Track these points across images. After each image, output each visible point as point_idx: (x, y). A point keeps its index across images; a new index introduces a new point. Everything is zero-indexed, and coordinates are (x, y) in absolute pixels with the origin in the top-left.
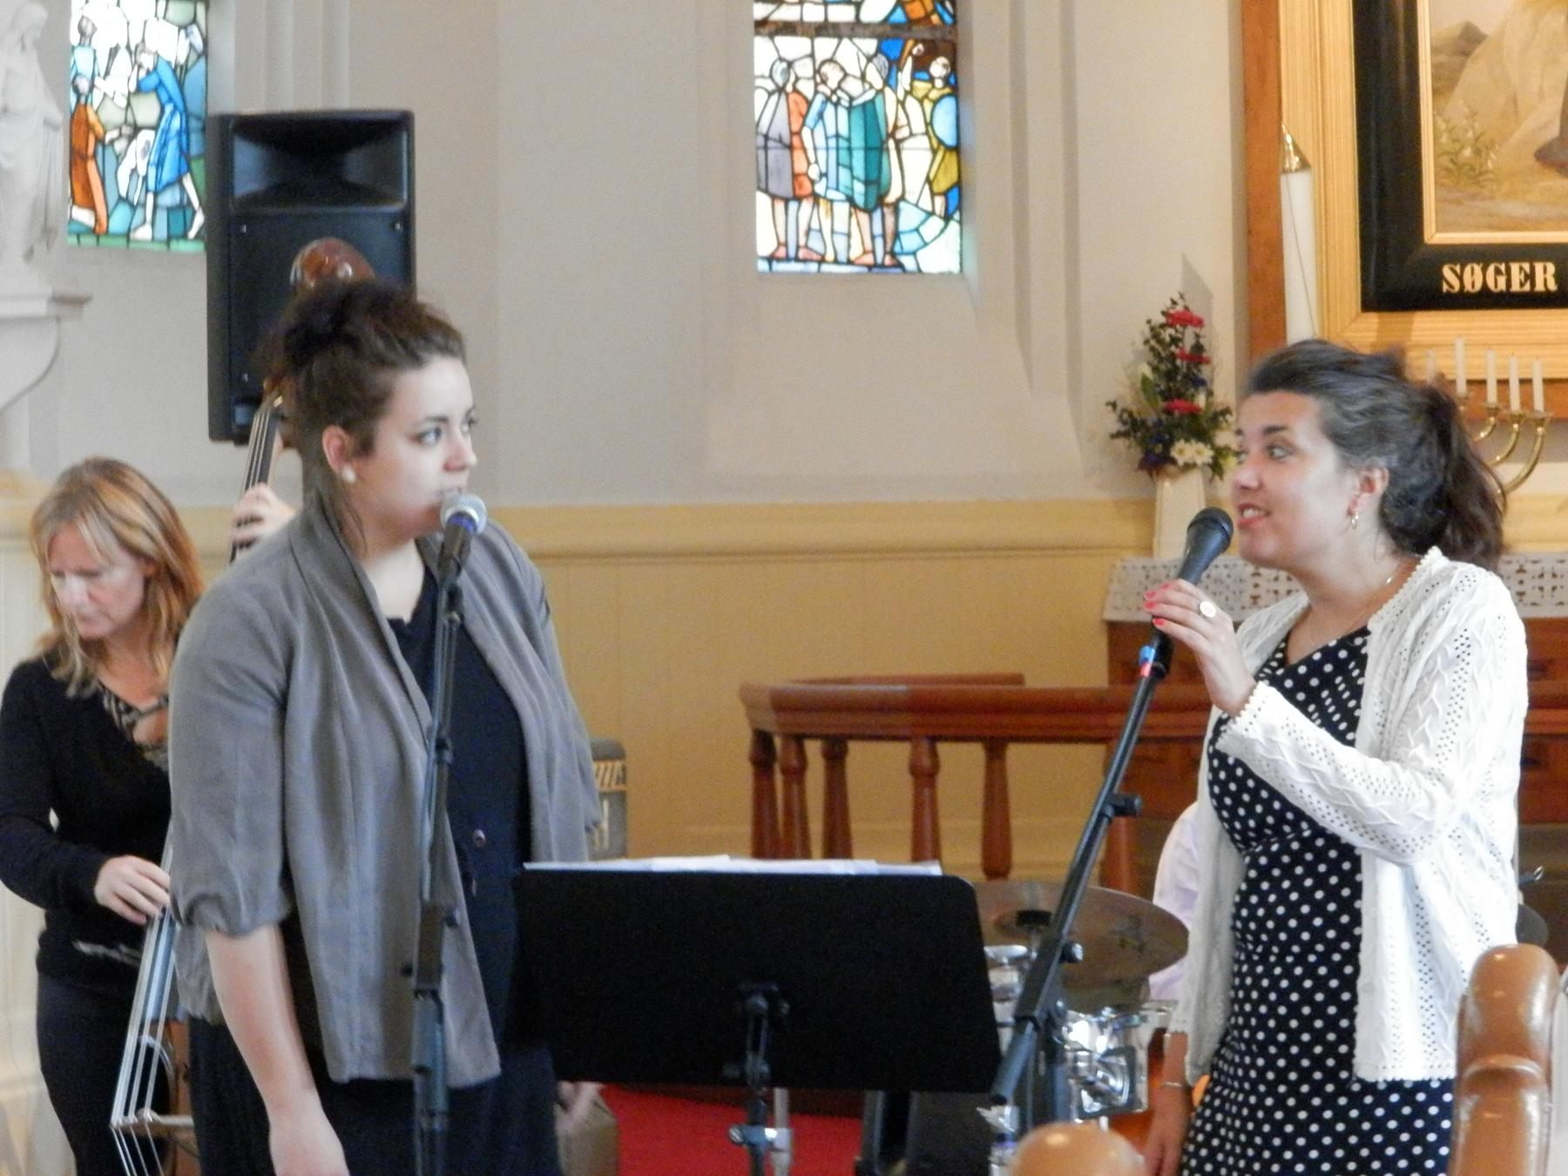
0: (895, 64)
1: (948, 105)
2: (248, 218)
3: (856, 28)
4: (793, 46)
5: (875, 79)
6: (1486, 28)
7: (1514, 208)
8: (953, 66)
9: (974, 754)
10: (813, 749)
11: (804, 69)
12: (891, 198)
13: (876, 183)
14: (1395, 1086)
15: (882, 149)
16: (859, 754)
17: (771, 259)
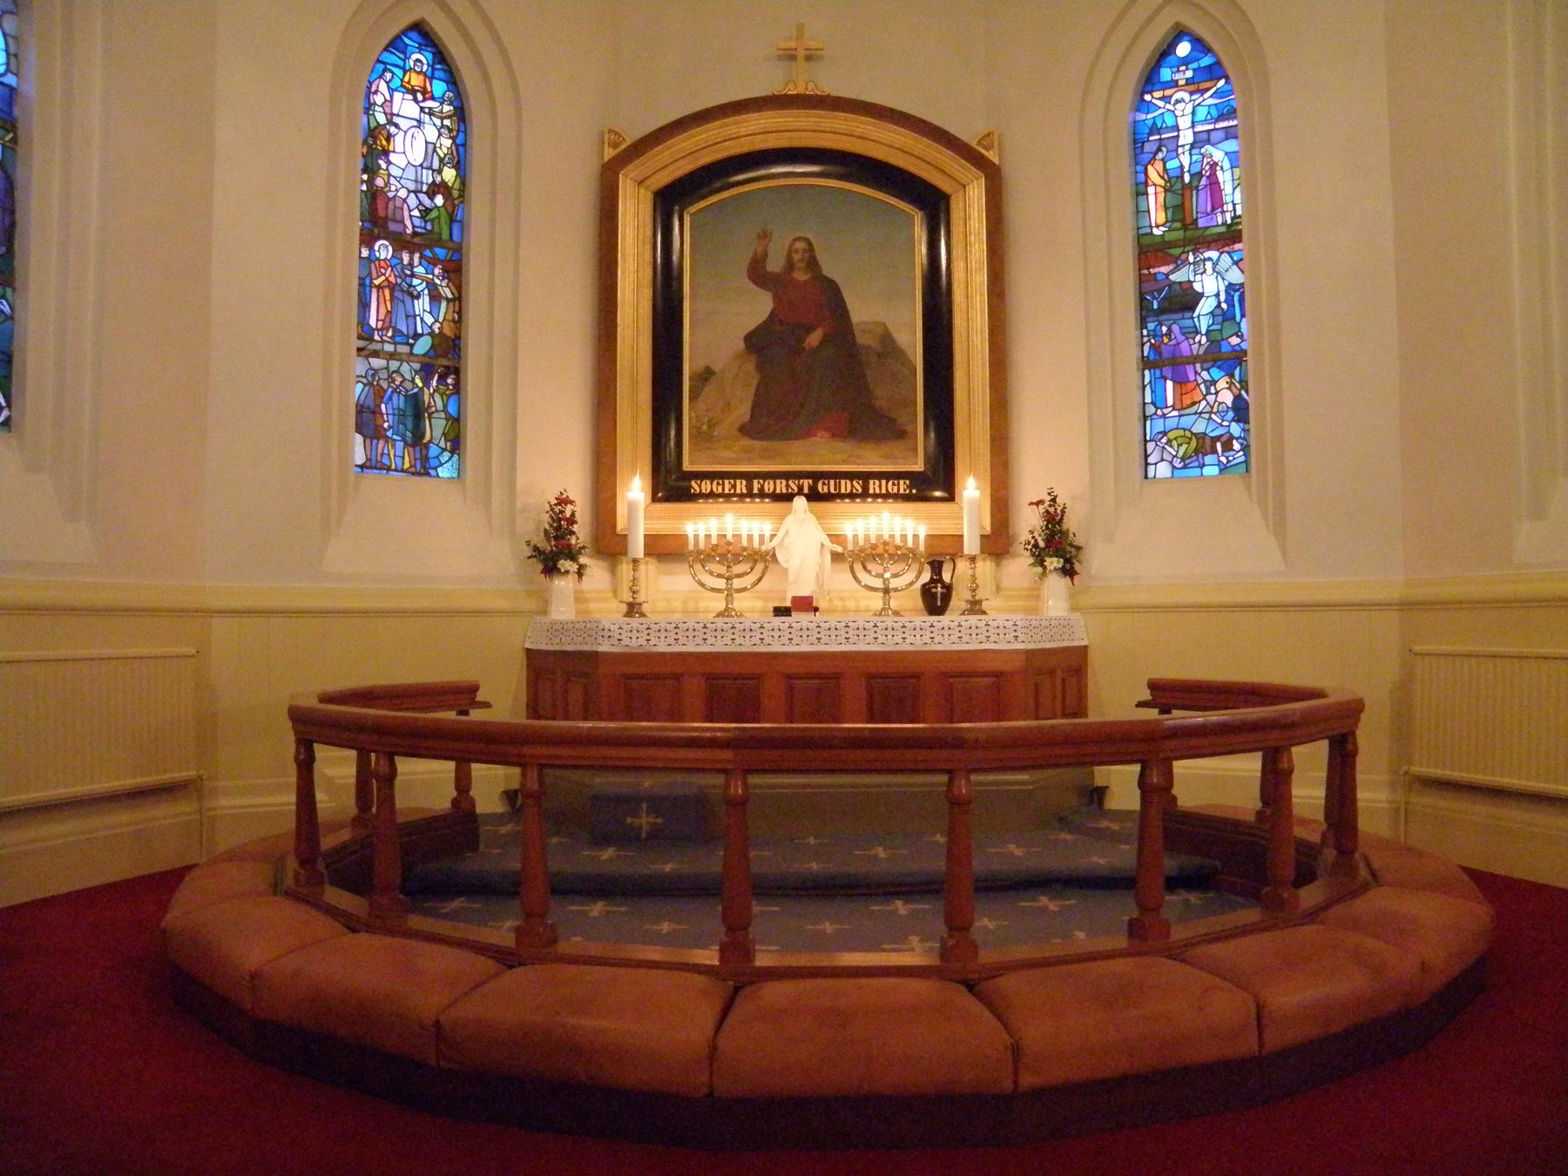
6: (717, 368)
11: (384, 375)
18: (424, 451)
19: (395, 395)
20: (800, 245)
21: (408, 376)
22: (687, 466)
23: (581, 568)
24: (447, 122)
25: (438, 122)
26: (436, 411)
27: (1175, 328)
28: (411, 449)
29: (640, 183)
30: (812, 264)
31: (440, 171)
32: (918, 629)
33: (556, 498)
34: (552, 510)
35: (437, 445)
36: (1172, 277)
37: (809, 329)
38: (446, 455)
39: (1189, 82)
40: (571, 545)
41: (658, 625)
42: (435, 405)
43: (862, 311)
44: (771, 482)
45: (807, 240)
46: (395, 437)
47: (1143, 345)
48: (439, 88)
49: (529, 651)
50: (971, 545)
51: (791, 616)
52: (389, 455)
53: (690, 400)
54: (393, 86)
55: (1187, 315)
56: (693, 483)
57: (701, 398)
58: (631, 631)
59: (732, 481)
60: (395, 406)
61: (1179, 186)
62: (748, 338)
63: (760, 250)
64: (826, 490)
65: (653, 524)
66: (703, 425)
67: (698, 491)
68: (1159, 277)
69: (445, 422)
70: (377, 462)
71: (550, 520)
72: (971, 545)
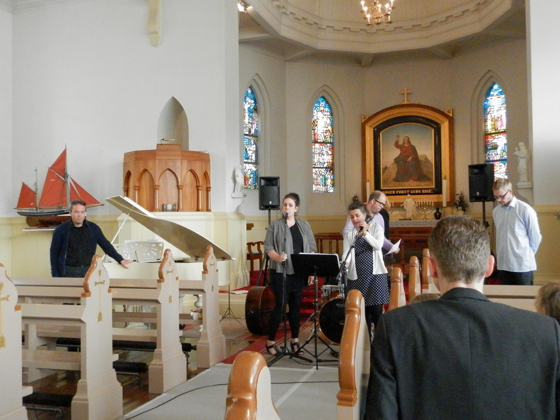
0: (327, 171)
1: (332, 175)
2: (263, 188)
3: (323, 168)
4: (317, 169)
5: (325, 173)
6: (388, 166)
7: (391, 185)
8: (333, 171)
9: (335, 241)
10: (319, 240)
11: (318, 172)
12: (327, 184)
13: (325, 183)
14: (379, 275)
15: (326, 180)
16: (323, 241)
17: (315, 191)
20: (406, 138)
21: (323, 172)
24: (329, 117)
25: (327, 117)
27: (493, 153)
29: (370, 127)
30: (409, 142)
31: (327, 127)
36: (493, 141)
37: (409, 157)
39: (497, 95)
43: (421, 152)
45: (408, 137)
47: (486, 157)
48: (327, 109)
50: (444, 205)
51: (85, 221)
54: (317, 111)
55: (496, 150)
61: (494, 120)
62: (395, 159)
63: (397, 140)
68: (490, 141)
72: (444, 205)
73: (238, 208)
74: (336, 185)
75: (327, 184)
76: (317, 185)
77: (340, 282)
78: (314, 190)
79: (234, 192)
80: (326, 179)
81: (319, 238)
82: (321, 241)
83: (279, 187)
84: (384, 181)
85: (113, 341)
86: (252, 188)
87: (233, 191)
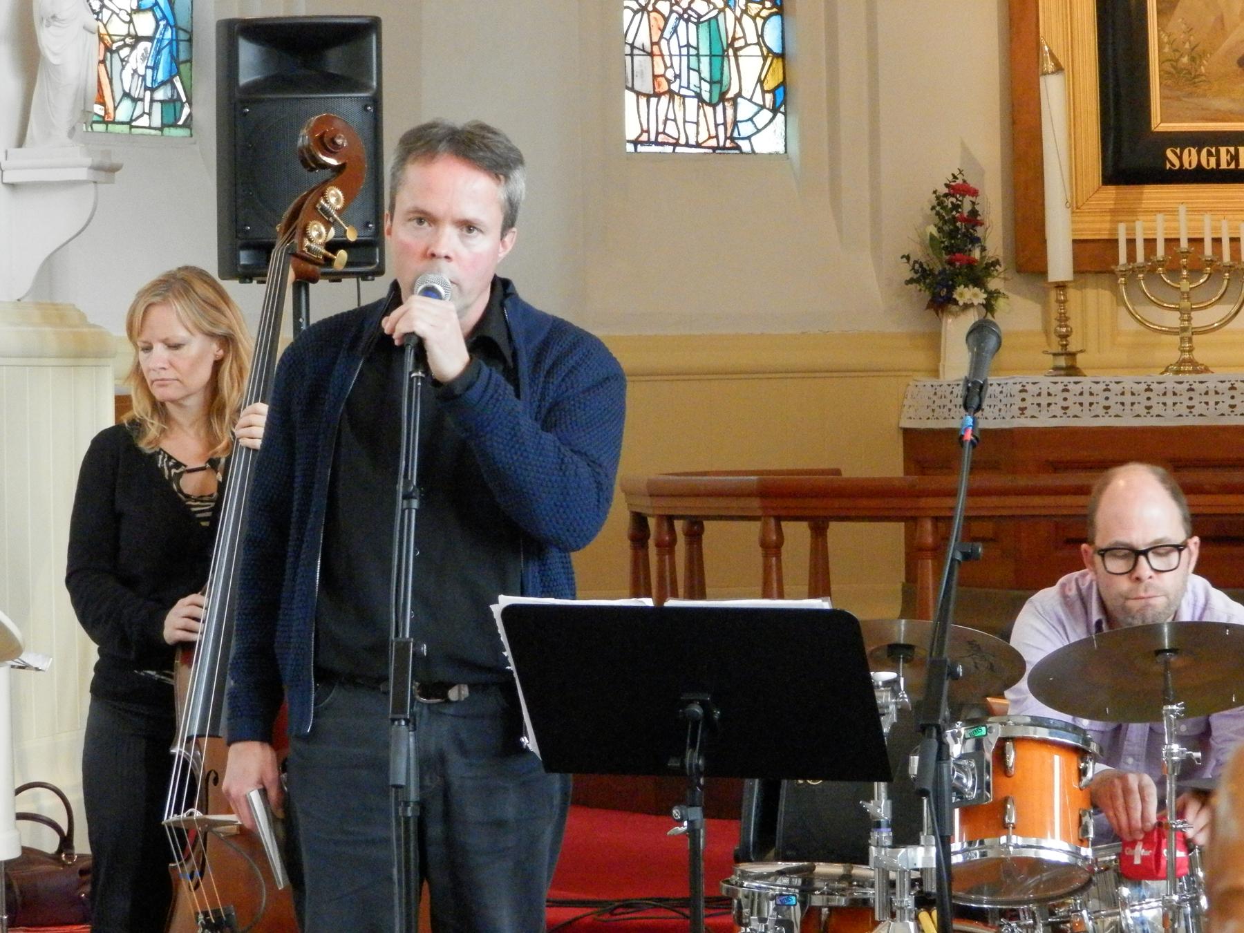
1: (776, 20)
7: (1221, 104)
10: (679, 525)
15: (723, 56)
17: (636, 143)
18: (730, 112)
19: (682, 23)
22: (1159, 124)
23: (992, 296)
26: (747, 45)
28: (709, 110)
32: (1212, 393)
33: (947, 186)
34: (940, 203)
35: (750, 100)
38: (766, 115)
40: (975, 261)
41: (1204, 385)
42: (744, 37)
44: (1194, 151)
46: (683, 92)
49: (907, 432)
52: (675, 120)
53: (1160, 12)
56: (1169, 153)
57: (1178, 11)
58: (1123, 394)
59: (1232, 149)
60: (683, 42)
64: (1213, 164)
65: (1093, 222)
66: (1182, 56)
67: (1178, 166)
69: (761, 60)
70: (658, 134)
71: (937, 220)
73: (49, 269)
74: (801, 92)
75: (730, 95)
76: (658, 95)
77: (885, 835)
78: (632, 132)
79: (21, 143)
80: (724, 51)
81: (1191, 240)
82: (695, 535)
83: (376, 101)
84: (1173, 74)
85: (1075, 242)
86: (144, 121)
87: (14, 136)
